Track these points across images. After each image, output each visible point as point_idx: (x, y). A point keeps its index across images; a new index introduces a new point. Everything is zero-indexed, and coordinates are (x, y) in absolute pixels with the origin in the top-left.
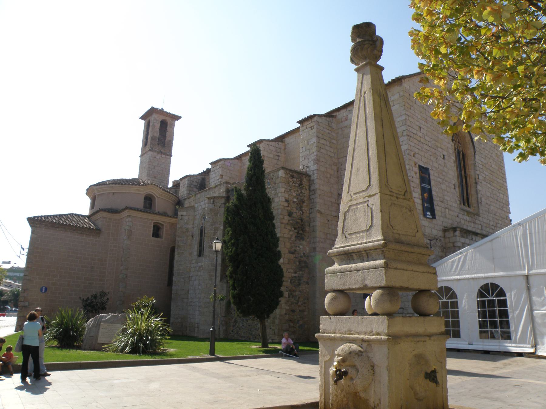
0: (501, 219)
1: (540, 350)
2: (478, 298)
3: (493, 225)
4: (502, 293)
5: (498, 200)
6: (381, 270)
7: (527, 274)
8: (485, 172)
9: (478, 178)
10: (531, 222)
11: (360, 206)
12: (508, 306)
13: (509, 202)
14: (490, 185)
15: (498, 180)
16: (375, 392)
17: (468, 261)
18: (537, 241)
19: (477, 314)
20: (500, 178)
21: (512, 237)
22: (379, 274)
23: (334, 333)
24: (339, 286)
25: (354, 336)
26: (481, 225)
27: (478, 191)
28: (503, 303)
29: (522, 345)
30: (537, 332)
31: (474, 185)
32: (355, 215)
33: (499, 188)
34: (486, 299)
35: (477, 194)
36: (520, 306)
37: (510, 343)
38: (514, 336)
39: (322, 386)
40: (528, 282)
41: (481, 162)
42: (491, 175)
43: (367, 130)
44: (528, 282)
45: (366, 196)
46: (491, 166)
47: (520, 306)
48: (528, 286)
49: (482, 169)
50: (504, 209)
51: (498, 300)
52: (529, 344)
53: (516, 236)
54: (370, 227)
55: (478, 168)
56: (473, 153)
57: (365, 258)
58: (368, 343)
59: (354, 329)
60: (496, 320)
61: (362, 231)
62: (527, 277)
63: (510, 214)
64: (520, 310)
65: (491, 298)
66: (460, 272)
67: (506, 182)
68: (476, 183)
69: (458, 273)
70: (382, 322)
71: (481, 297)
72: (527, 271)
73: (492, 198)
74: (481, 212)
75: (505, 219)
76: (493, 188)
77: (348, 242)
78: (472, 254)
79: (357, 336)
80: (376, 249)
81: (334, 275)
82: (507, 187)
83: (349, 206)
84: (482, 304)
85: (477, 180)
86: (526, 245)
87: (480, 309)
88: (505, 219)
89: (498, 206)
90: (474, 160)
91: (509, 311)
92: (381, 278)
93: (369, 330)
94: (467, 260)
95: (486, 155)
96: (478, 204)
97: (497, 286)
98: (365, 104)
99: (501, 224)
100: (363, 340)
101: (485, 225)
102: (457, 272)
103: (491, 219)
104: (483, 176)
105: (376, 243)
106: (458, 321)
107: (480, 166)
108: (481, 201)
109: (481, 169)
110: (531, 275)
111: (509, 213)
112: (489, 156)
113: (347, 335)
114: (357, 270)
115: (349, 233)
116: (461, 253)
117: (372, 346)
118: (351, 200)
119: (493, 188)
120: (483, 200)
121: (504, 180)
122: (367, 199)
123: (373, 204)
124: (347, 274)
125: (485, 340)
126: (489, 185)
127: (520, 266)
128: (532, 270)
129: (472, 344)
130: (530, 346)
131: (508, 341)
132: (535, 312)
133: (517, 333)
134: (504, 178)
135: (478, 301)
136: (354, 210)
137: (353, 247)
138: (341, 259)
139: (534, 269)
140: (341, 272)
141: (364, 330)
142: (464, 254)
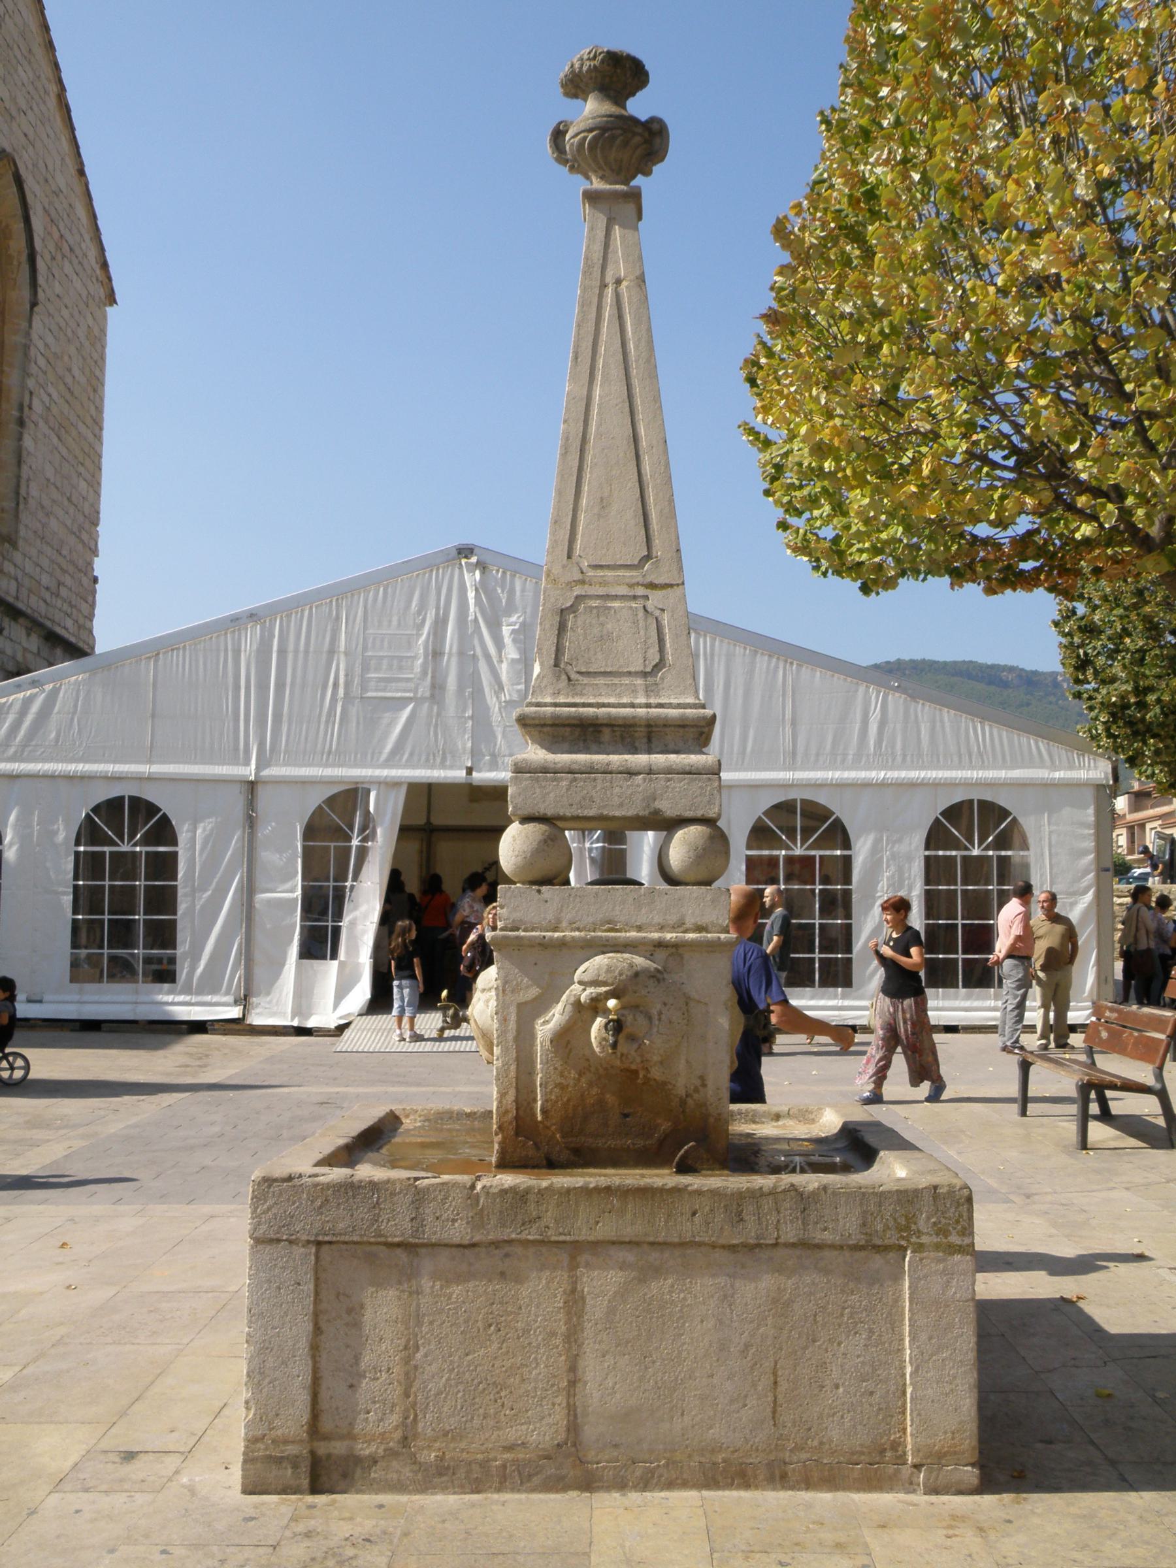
0: (71, 569)
1: (258, 1010)
2: (78, 843)
3: (47, 589)
4: (164, 831)
5: (74, 499)
6: (709, 779)
7: (252, 778)
8: (51, 390)
9: (30, 408)
10: (289, 616)
11: (616, 604)
12: (180, 875)
13: (98, 513)
14: (59, 438)
15: (82, 428)
16: (687, 1062)
17: (59, 713)
18: (299, 680)
19: (69, 898)
20: (89, 421)
21: (222, 654)
22: (701, 787)
23: (555, 930)
24: (562, 807)
25: (628, 934)
26: (16, 580)
27: (24, 453)
28: (165, 866)
29: (208, 998)
30: (258, 956)
31: (13, 427)
32: (602, 625)
33: (81, 459)
34: (107, 849)
35: (19, 463)
36: (218, 875)
37: (169, 993)
38: (185, 971)
39: (507, 1071)
40: (251, 804)
41: (46, 345)
42: (67, 406)
43: (630, 396)
44: (251, 804)
45: (638, 584)
46: (69, 370)
47: (218, 875)
48: (250, 817)
49: (45, 373)
50: (85, 536)
51: (147, 853)
52: (227, 993)
53: (237, 652)
54: (656, 666)
55: (33, 369)
56: (28, 307)
57: (641, 743)
58: (674, 950)
59: (622, 918)
60: (134, 920)
61: (629, 673)
62: (252, 787)
63: (97, 556)
64: (215, 891)
65: (125, 848)
66: (23, 751)
67: (99, 438)
68: (21, 423)
69: (16, 752)
70: (713, 901)
71: (93, 843)
72: (253, 766)
73: (57, 488)
74: (22, 532)
75: (80, 571)
76: (64, 452)
77: (581, 694)
78: (78, 691)
79: (633, 934)
80: (683, 726)
81: (546, 779)
82: (100, 456)
83: (577, 597)
84: (89, 866)
85: (26, 409)
86: (263, 687)
87: (81, 883)
88: (80, 571)
89: (69, 523)
90: (28, 334)
91: (181, 892)
92: (706, 799)
93: (673, 919)
94: (56, 710)
95: (63, 324)
96: (18, 504)
97: (152, 809)
98: (621, 318)
99: (70, 589)
100: (660, 944)
101: (26, 582)
102: (12, 750)
103: (45, 563)
104: (43, 402)
105: (688, 711)
106: (172, 925)
107: (42, 362)
108: (28, 494)
109: (40, 373)
110: (264, 782)
111: (95, 552)
112: (69, 334)
113: (599, 934)
114: (631, 773)
115: (584, 670)
116: (34, 683)
117: (682, 958)
118: (582, 582)
119: (64, 452)
120: (34, 491)
121: (97, 431)
122: (640, 591)
123: (663, 610)
124: (595, 780)
125: (88, 987)
126: (55, 440)
127: (236, 749)
128: (268, 765)
129: (40, 1001)
130: (230, 999)
131: (166, 986)
132: (262, 897)
133: (196, 959)
134: (97, 424)
135: (77, 854)
136: (595, 611)
137: (613, 710)
138: (554, 737)
139: (276, 765)
140: (571, 772)
141: (658, 919)
142: (48, 687)
